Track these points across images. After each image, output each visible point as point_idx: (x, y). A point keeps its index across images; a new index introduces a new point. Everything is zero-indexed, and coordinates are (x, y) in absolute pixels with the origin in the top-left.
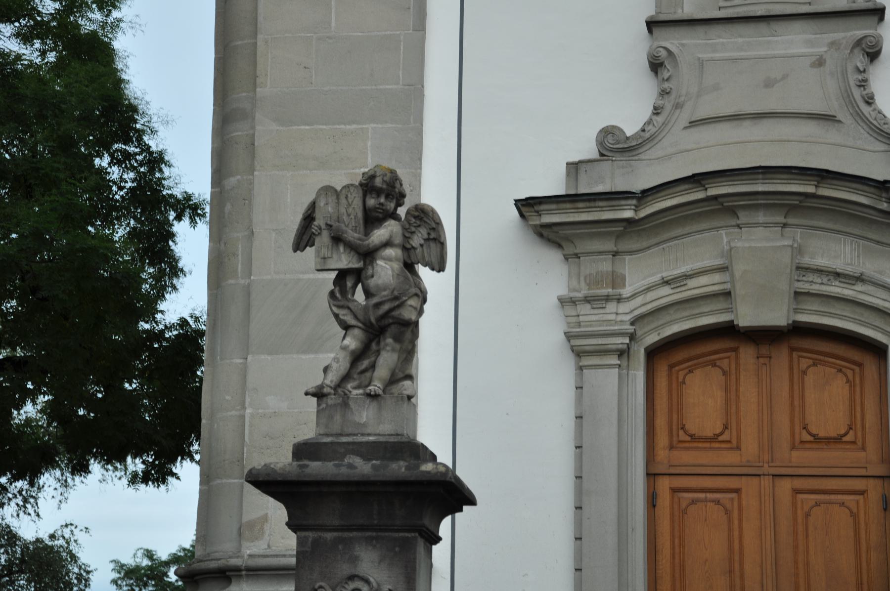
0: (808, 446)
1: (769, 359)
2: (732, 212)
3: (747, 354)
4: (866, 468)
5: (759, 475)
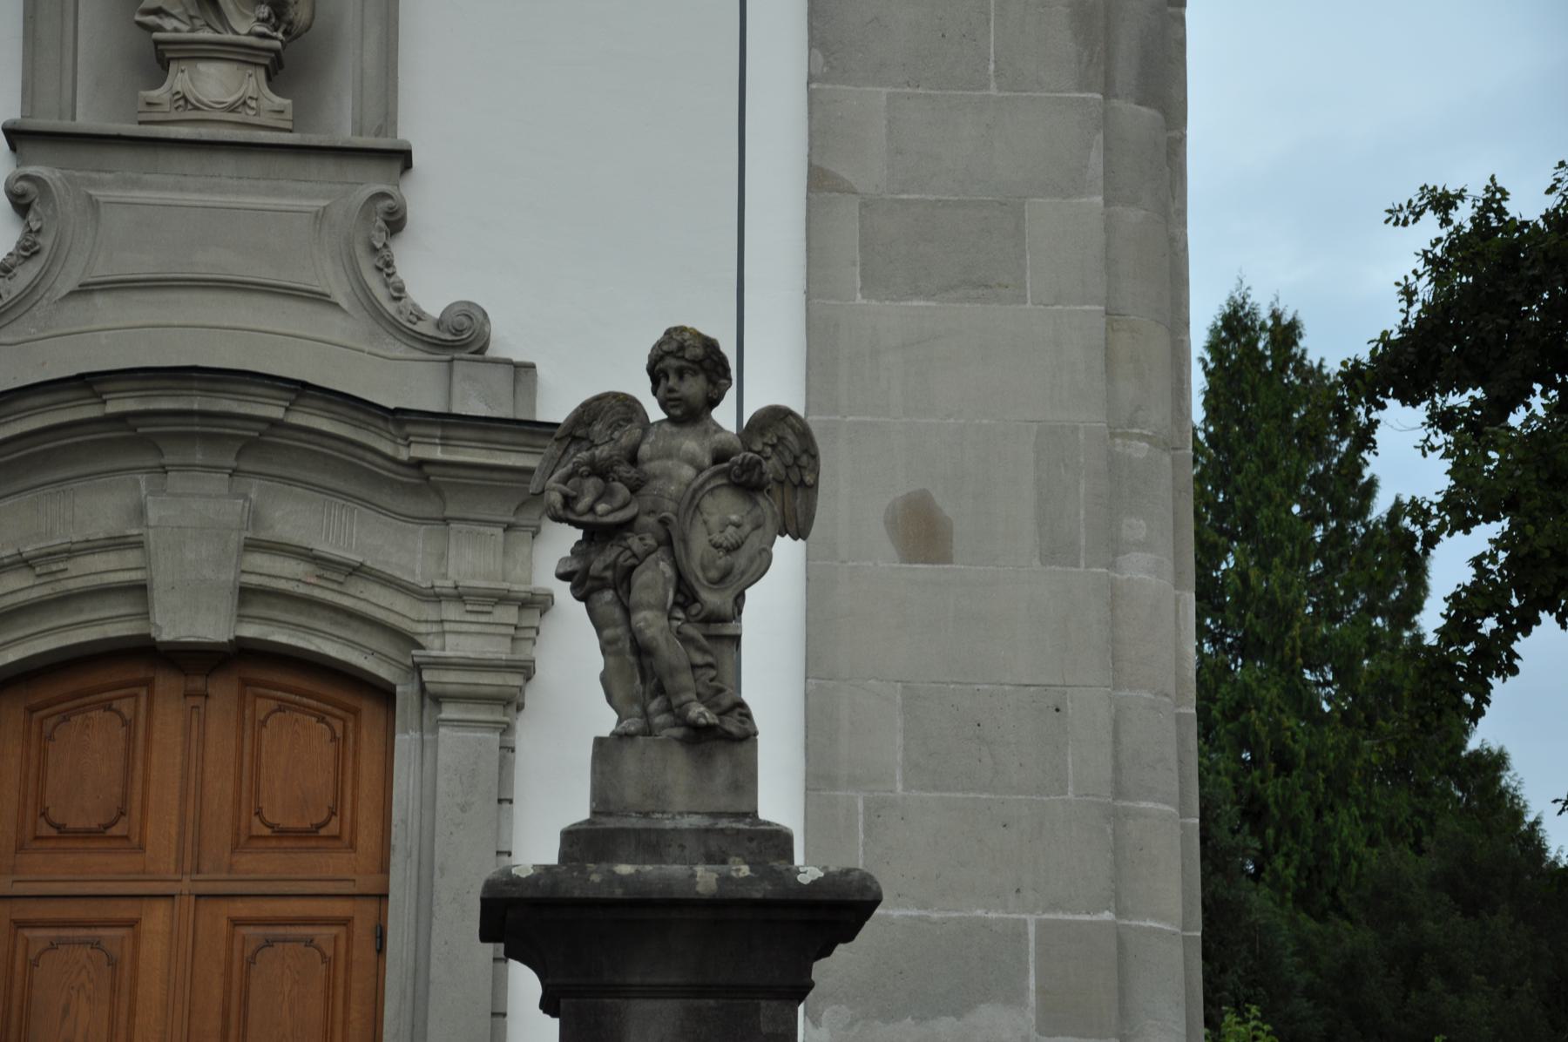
0: (261, 844)
1: (203, 698)
2: (150, 444)
3: (167, 684)
4: (354, 880)
5: (172, 896)
